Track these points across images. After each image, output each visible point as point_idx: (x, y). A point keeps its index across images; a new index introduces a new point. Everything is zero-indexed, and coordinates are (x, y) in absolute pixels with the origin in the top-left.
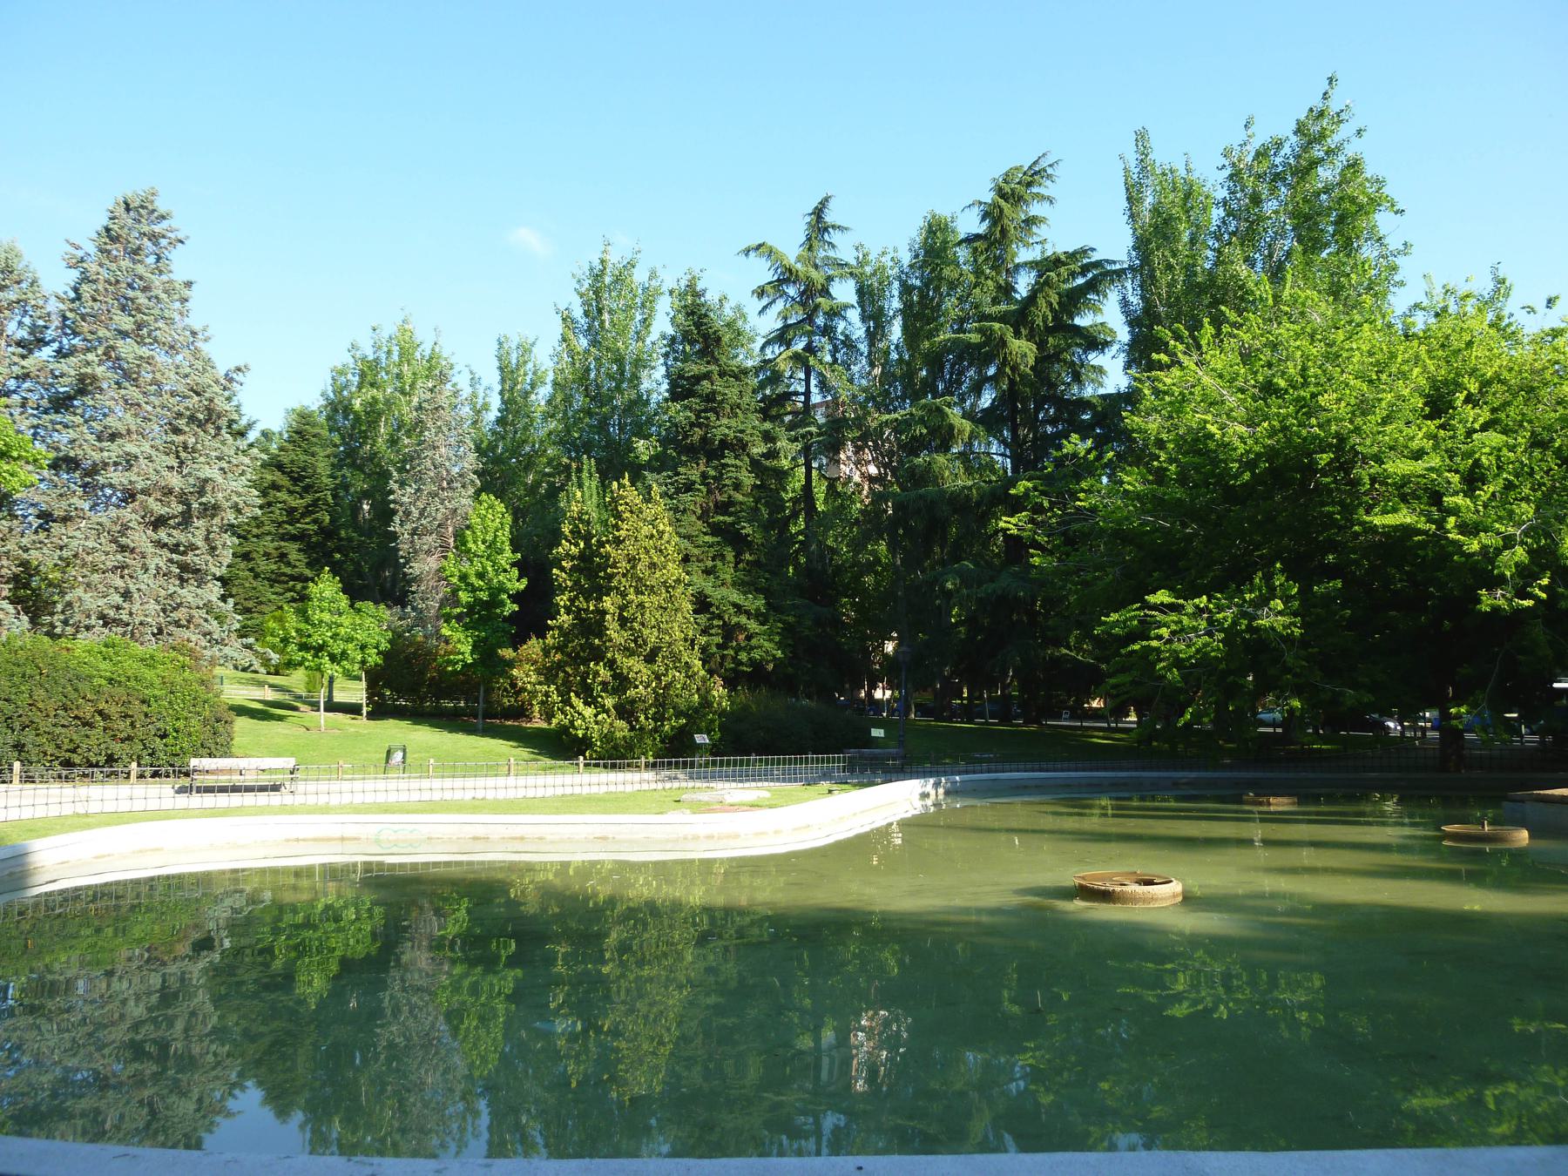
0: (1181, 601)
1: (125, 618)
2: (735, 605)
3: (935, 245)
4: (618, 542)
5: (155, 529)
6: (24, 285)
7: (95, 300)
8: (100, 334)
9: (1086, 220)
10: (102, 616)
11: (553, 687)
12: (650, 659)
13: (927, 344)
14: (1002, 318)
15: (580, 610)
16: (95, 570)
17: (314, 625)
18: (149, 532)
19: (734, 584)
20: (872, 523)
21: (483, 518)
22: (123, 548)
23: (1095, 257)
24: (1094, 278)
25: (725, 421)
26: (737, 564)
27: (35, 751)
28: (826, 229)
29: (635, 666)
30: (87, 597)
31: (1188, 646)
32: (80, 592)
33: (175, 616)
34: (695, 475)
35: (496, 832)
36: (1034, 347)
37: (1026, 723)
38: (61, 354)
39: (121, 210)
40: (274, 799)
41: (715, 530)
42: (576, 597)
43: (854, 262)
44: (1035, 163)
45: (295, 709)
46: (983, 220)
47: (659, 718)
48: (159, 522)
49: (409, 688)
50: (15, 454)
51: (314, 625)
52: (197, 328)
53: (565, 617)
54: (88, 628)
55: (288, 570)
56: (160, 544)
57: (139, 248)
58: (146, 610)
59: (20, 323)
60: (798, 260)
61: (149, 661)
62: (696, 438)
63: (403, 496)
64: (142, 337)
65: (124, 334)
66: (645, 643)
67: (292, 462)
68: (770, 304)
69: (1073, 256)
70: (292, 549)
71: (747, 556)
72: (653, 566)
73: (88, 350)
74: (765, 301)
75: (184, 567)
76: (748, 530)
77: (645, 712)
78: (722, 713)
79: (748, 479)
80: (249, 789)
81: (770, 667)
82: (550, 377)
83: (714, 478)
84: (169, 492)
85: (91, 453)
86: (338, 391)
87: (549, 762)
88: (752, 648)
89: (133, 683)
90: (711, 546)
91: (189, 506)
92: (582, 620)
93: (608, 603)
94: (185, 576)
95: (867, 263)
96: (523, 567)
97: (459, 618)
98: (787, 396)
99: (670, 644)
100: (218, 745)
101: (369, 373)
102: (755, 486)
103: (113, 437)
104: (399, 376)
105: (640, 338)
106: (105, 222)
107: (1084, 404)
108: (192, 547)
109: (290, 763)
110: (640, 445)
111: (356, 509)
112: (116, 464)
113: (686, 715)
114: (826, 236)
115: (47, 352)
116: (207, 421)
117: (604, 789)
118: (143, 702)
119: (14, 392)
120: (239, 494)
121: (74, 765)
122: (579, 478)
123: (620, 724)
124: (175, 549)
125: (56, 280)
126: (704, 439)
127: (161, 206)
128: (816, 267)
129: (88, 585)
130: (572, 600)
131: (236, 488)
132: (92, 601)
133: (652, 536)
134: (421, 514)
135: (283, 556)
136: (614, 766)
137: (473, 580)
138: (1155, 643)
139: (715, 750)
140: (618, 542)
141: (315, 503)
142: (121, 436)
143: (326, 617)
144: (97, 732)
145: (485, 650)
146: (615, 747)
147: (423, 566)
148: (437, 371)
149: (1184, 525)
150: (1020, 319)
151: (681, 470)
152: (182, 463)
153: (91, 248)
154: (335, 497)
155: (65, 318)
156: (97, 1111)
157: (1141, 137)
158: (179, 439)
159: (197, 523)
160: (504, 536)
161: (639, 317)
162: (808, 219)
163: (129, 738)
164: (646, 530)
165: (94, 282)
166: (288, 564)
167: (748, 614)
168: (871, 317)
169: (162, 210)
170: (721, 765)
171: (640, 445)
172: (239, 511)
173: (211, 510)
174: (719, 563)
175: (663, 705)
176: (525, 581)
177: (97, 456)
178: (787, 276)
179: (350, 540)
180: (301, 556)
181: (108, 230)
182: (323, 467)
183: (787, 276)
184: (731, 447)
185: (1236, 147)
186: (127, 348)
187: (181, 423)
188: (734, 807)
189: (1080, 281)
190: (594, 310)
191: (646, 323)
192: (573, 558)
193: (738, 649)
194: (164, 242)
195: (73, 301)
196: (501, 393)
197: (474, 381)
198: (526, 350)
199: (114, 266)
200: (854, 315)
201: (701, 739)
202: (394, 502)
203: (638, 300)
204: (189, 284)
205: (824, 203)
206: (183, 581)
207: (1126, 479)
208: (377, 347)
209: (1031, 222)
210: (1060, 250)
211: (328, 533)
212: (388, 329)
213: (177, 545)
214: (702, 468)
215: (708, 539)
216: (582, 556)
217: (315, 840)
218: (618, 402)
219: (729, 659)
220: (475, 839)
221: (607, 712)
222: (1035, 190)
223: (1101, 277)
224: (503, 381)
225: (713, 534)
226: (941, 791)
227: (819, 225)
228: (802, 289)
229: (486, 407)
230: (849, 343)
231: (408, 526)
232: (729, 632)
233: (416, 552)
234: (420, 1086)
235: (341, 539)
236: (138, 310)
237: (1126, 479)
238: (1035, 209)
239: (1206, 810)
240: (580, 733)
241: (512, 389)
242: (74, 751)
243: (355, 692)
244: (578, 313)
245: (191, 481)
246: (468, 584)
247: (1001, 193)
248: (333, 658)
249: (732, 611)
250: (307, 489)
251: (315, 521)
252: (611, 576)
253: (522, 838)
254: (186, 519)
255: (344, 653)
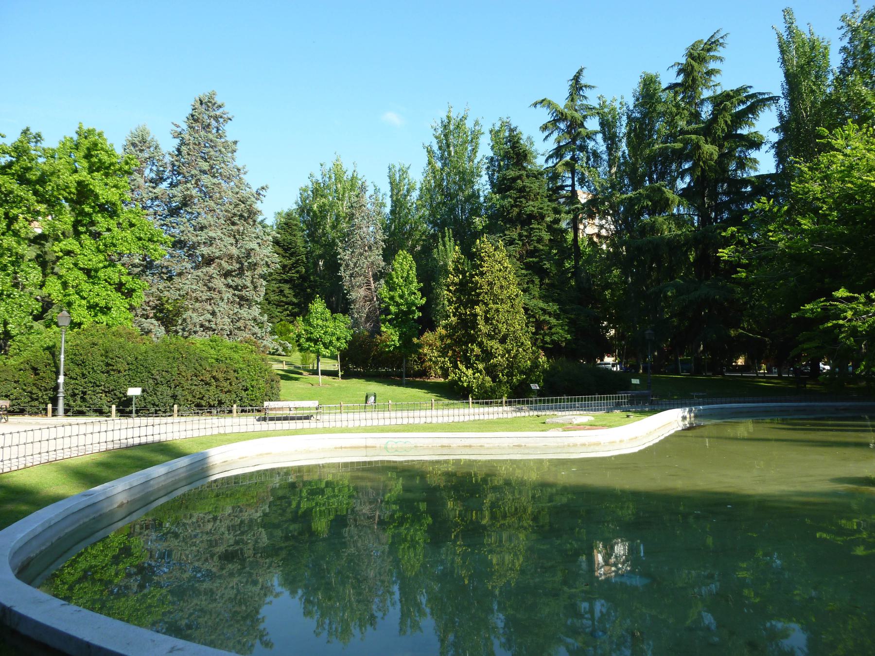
0: (856, 295)
1: (214, 326)
2: (542, 309)
3: (648, 91)
4: (482, 274)
5: (225, 278)
6: (152, 149)
7: (189, 154)
8: (192, 172)
9: (751, 67)
10: (202, 326)
11: (447, 359)
12: (503, 341)
13: (648, 151)
14: (695, 132)
15: (461, 314)
16: (197, 300)
17: (314, 327)
18: (223, 279)
19: (540, 298)
20: (614, 258)
21: (401, 264)
22: (210, 289)
23: (751, 91)
24: (753, 104)
25: (531, 203)
26: (541, 285)
27: (182, 399)
28: (581, 88)
29: (494, 345)
30: (194, 315)
31: (864, 323)
32: (190, 313)
33: (238, 324)
34: (515, 235)
35: (455, 443)
36: (717, 149)
37: (714, 375)
38: (172, 185)
39: (198, 105)
40: (306, 424)
41: (528, 266)
42: (459, 307)
43: (598, 107)
44: (712, 37)
45: (301, 374)
46: (678, 74)
47: (510, 375)
48: (227, 274)
49: (365, 362)
50: (155, 239)
51: (314, 327)
52: (240, 167)
53: (453, 318)
54: (195, 332)
55: (284, 299)
56: (229, 286)
57: (209, 125)
58: (223, 322)
59: (151, 170)
60: (566, 107)
61: (235, 349)
62: (515, 213)
63: (345, 255)
64: (214, 174)
65: (204, 172)
66: (500, 332)
67: (284, 240)
68: (550, 134)
69: (738, 91)
70: (286, 287)
71: (547, 281)
72: (502, 287)
73: (186, 182)
74: (547, 133)
75: (241, 298)
76: (547, 266)
77: (502, 371)
78: (544, 371)
79: (546, 236)
80: (293, 419)
81: (564, 344)
82: (418, 186)
83: (526, 236)
84: (231, 257)
85: (192, 238)
86: (303, 200)
87: (446, 401)
88: (553, 334)
89: (228, 361)
90: (526, 276)
91: (242, 264)
92: (462, 320)
93: (478, 309)
94: (242, 303)
95: (605, 107)
96: (424, 292)
97: (390, 321)
98: (562, 187)
99: (514, 332)
100: (274, 396)
101: (317, 192)
102: (550, 240)
103: (202, 228)
104: (336, 191)
105: (471, 160)
106: (190, 111)
107: (746, 182)
108: (245, 287)
109: (314, 404)
110: (477, 220)
111: (316, 264)
112: (204, 243)
113: (524, 373)
114: (581, 92)
115: (165, 185)
116: (248, 217)
117: (496, 416)
118: (235, 371)
119: (150, 207)
120: (268, 257)
121: (202, 406)
122: (443, 241)
123: (488, 378)
124: (236, 288)
125: (168, 145)
126: (519, 214)
127: (218, 100)
128: (576, 110)
129: (194, 309)
130: (456, 309)
131: (267, 255)
132: (197, 318)
133: (501, 270)
134: (355, 265)
135: (281, 291)
136: (487, 403)
137: (397, 299)
138: (841, 322)
139: (540, 393)
140: (482, 274)
141: (297, 261)
142: (206, 227)
143: (320, 322)
144: (213, 388)
145: (406, 339)
146: (486, 392)
147: (358, 294)
148: (355, 185)
149: (842, 249)
150: (708, 130)
151: (507, 232)
152: (237, 241)
153: (185, 126)
154: (307, 258)
155: (173, 165)
156: (211, 591)
157: (787, 12)
158: (235, 228)
159: (247, 273)
160: (413, 273)
161: (470, 148)
162: (570, 83)
163: (229, 391)
164: (497, 267)
165: (188, 144)
166: (284, 296)
167: (550, 314)
168: (610, 139)
169: (219, 103)
170: (556, 402)
171: (477, 220)
172: (268, 266)
173: (253, 266)
174: (531, 286)
175: (512, 367)
176: (425, 299)
177: (195, 239)
178: (560, 117)
179: (315, 281)
180: (291, 291)
181: (192, 116)
182: (300, 242)
183: (560, 117)
184: (535, 218)
185: (849, 14)
186: (206, 179)
187: (236, 219)
188: (580, 427)
189: (742, 107)
190: (444, 146)
191: (474, 151)
192: (456, 284)
193: (545, 334)
194: (221, 120)
195: (177, 156)
196: (391, 196)
197: (377, 190)
198: (404, 172)
199: (197, 135)
200: (599, 137)
201: (535, 387)
202: (341, 259)
203: (469, 138)
204: (235, 143)
205: (580, 72)
206: (241, 306)
207: (803, 222)
208: (324, 175)
209: (710, 73)
210: (728, 89)
211: (304, 278)
212: (329, 165)
213: (237, 286)
214: (518, 231)
215: (523, 271)
216: (461, 283)
217: (351, 447)
218: (461, 197)
219: (539, 341)
220: (442, 446)
221: (480, 372)
222: (712, 54)
223: (758, 103)
224: (392, 190)
225: (526, 269)
226: (692, 415)
227: (577, 86)
228: (568, 125)
229: (383, 205)
230: (596, 155)
231: (348, 273)
232: (539, 325)
233: (352, 286)
234: (366, 579)
235: (311, 281)
236: (210, 158)
237: (803, 222)
238: (712, 65)
239: (828, 425)
240: (465, 384)
241: (397, 194)
242: (202, 399)
243: (334, 365)
244: (435, 148)
245: (243, 250)
246: (395, 302)
247: (691, 56)
248: (324, 344)
249: (541, 312)
250: (292, 255)
251: (297, 272)
252: (480, 294)
253: (470, 446)
254: (241, 272)
255: (331, 342)
